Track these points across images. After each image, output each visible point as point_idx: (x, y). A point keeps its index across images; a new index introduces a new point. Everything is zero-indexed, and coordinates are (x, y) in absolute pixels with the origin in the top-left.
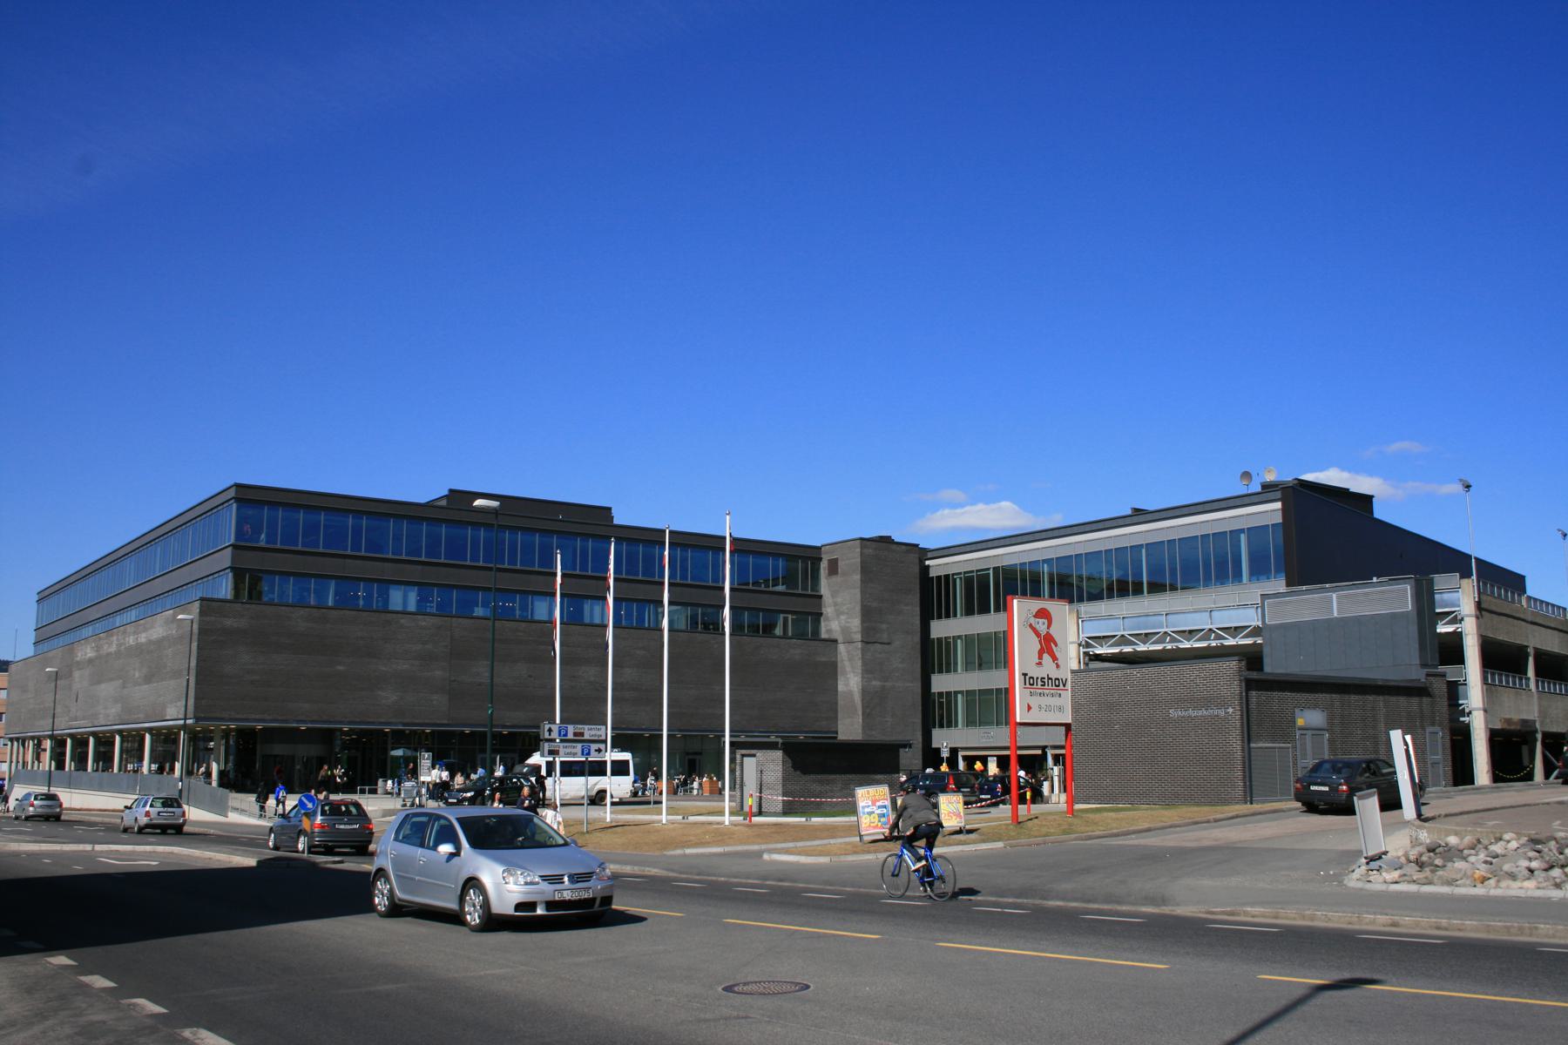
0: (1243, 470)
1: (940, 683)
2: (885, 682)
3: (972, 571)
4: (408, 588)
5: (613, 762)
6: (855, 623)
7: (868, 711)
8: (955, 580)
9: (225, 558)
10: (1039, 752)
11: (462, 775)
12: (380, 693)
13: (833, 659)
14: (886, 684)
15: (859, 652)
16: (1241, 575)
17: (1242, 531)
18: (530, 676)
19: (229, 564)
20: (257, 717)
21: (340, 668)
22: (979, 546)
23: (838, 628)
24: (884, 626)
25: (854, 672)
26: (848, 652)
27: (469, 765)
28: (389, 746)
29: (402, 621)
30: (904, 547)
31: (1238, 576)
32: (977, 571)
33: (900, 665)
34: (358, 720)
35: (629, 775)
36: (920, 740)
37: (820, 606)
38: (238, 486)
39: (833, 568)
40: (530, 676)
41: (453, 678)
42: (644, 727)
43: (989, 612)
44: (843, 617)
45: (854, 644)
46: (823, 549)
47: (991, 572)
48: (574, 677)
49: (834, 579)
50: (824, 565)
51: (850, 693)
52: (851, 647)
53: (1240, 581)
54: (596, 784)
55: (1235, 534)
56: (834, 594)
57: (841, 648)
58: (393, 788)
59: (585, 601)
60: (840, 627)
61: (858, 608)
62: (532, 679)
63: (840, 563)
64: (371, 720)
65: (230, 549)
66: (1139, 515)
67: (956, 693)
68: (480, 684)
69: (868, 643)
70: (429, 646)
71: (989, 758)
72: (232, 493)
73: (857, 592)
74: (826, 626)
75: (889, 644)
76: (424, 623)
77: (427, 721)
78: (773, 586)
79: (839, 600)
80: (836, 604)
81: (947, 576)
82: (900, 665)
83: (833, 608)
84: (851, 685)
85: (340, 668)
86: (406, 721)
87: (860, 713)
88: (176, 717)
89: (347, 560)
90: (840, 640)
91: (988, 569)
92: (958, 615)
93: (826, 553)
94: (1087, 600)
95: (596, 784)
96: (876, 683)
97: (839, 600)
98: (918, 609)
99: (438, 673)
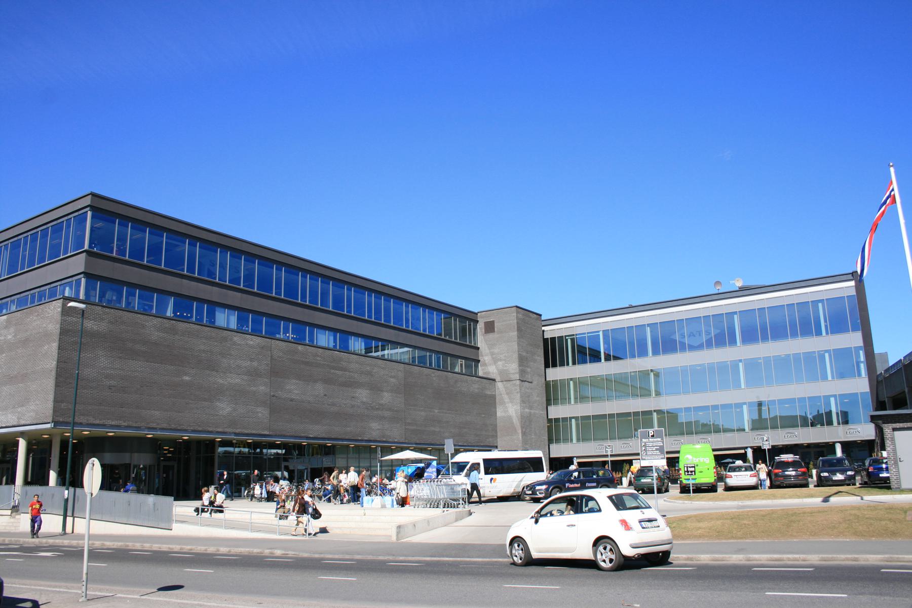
0: (715, 281)
1: (556, 412)
2: (531, 409)
3: (585, 334)
4: (231, 312)
5: (611, 461)
6: (513, 367)
7: (524, 430)
8: (567, 340)
9: (78, 264)
10: (743, 451)
11: (845, 477)
12: (218, 404)
13: (494, 393)
14: (532, 411)
15: (518, 388)
16: (736, 342)
17: (735, 313)
18: (325, 395)
19: (82, 270)
20: (113, 423)
21: (187, 378)
22: (675, 303)
23: (495, 371)
24: (529, 370)
25: (512, 402)
26: (506, 388)
27: (811, 463)
28: (110, 458)
29: (235, 339)
30: (535, 315)
31: (733, 342)
32: (588, 333)
33: (538, 399)
34: (200, 429)
35: (543, 471)
36: (88, 464)
37: (478, 355)
38: (94, 195)
39: (490, 327)
40: (325, 395)
41: (272, 394)
42: (396, 440)
43: (849, 331)
44: (500, 363)
45: (511, 382)
46: (479, 314)
47: (601, 334)
48: (353, 398)
49: (491, 335)
50: (480, 327)
51: (510, 418)
52: (509, 384)
53: (821, 334)
54: (521, 481)
55: (731, 315)
56: (491, 346)
57: (500, 385)
58: (261, 494)
59: (350, 337)
60: (498, 370)
61: (516, 356)
62: (327, 398)
63: (496, 325)
64: (211, 429)
65: (84, 254)
66: (745, 290)
67: (571, 418)
68: (292, 400)
69: (522, 381)
70: (255, 364)
71: (633, 461)
72: (88, 201)
73: (515, 346)
74: (483, 370)
75: (531, 382)
76: (252, 343)
77: (254, 432)
78: (375, 352)
79: (496, 351)
80: (492, 354)
81: (561, 338)
82: (538, 399)
83: (490, 357)
84: (510, 412)
85: (187, 378)
86: (238, 431)
87: (520, 431)
88: (15, 423)
89: (184, 280)
90: (498, 379)
91: (599, 332)
92: (824, 333)
93: (482, 317)
94: (560, 366)
95: (521, 481)
96: (527, 410)
97: (496, 351)
98: (543, 359)
99: (262, 388)
